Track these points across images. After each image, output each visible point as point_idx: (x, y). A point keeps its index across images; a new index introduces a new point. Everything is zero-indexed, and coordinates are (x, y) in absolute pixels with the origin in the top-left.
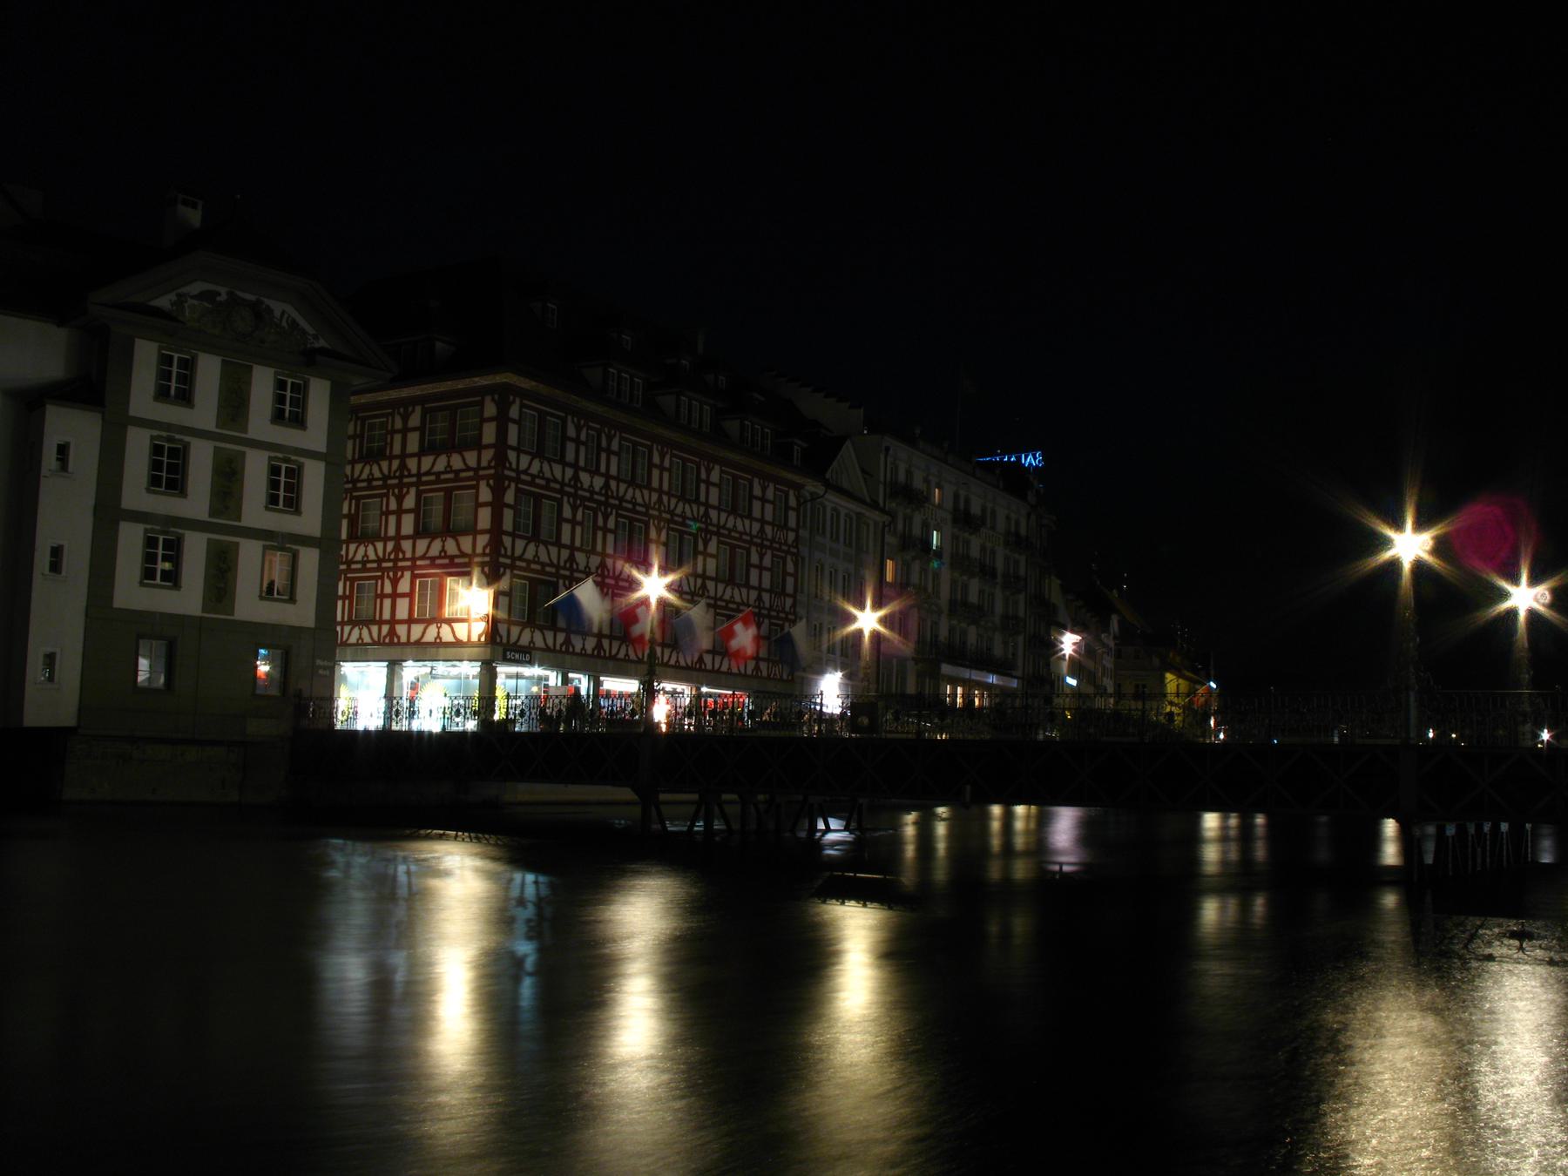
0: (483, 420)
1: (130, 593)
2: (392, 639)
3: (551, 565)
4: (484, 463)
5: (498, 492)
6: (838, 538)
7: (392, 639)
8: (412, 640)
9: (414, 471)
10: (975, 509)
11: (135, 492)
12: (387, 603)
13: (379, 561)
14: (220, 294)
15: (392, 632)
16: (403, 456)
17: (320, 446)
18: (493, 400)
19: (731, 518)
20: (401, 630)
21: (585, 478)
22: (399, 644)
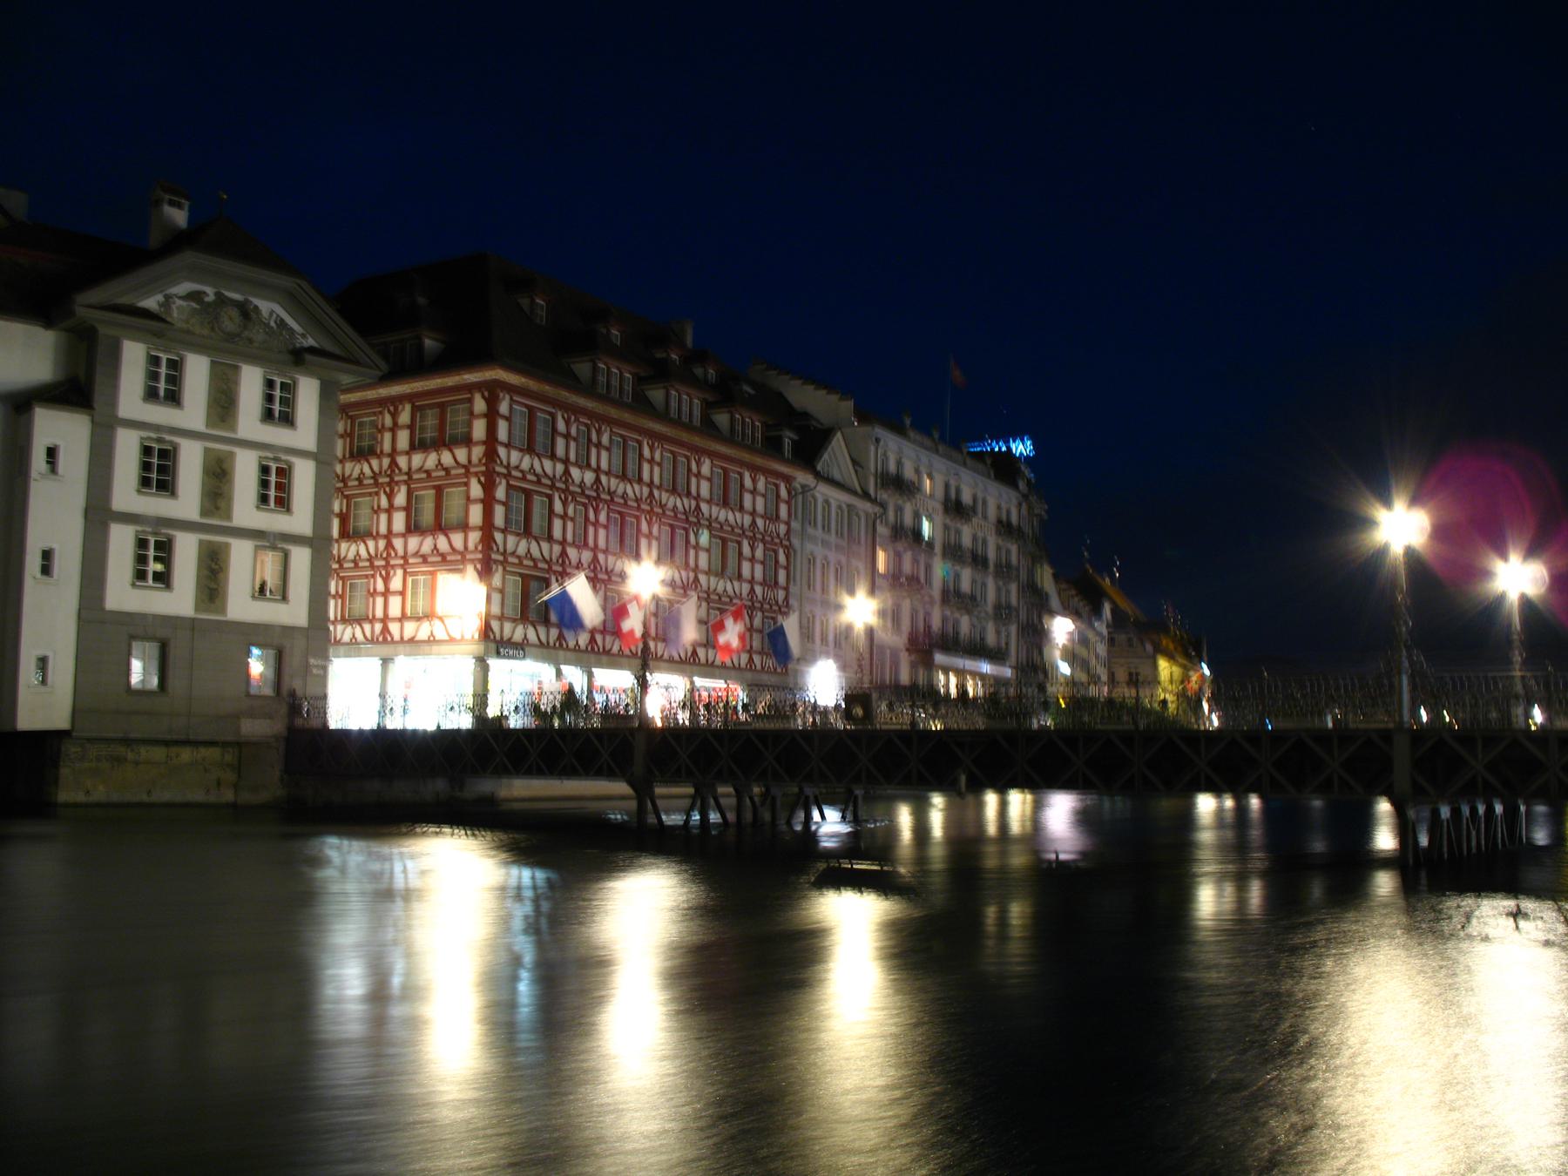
6: (829, 530)
8: (406, 638)
11: (126, 493)
12: (380, 601)
15: (385, 630)
18: (483, 397)
20: (394, 628)
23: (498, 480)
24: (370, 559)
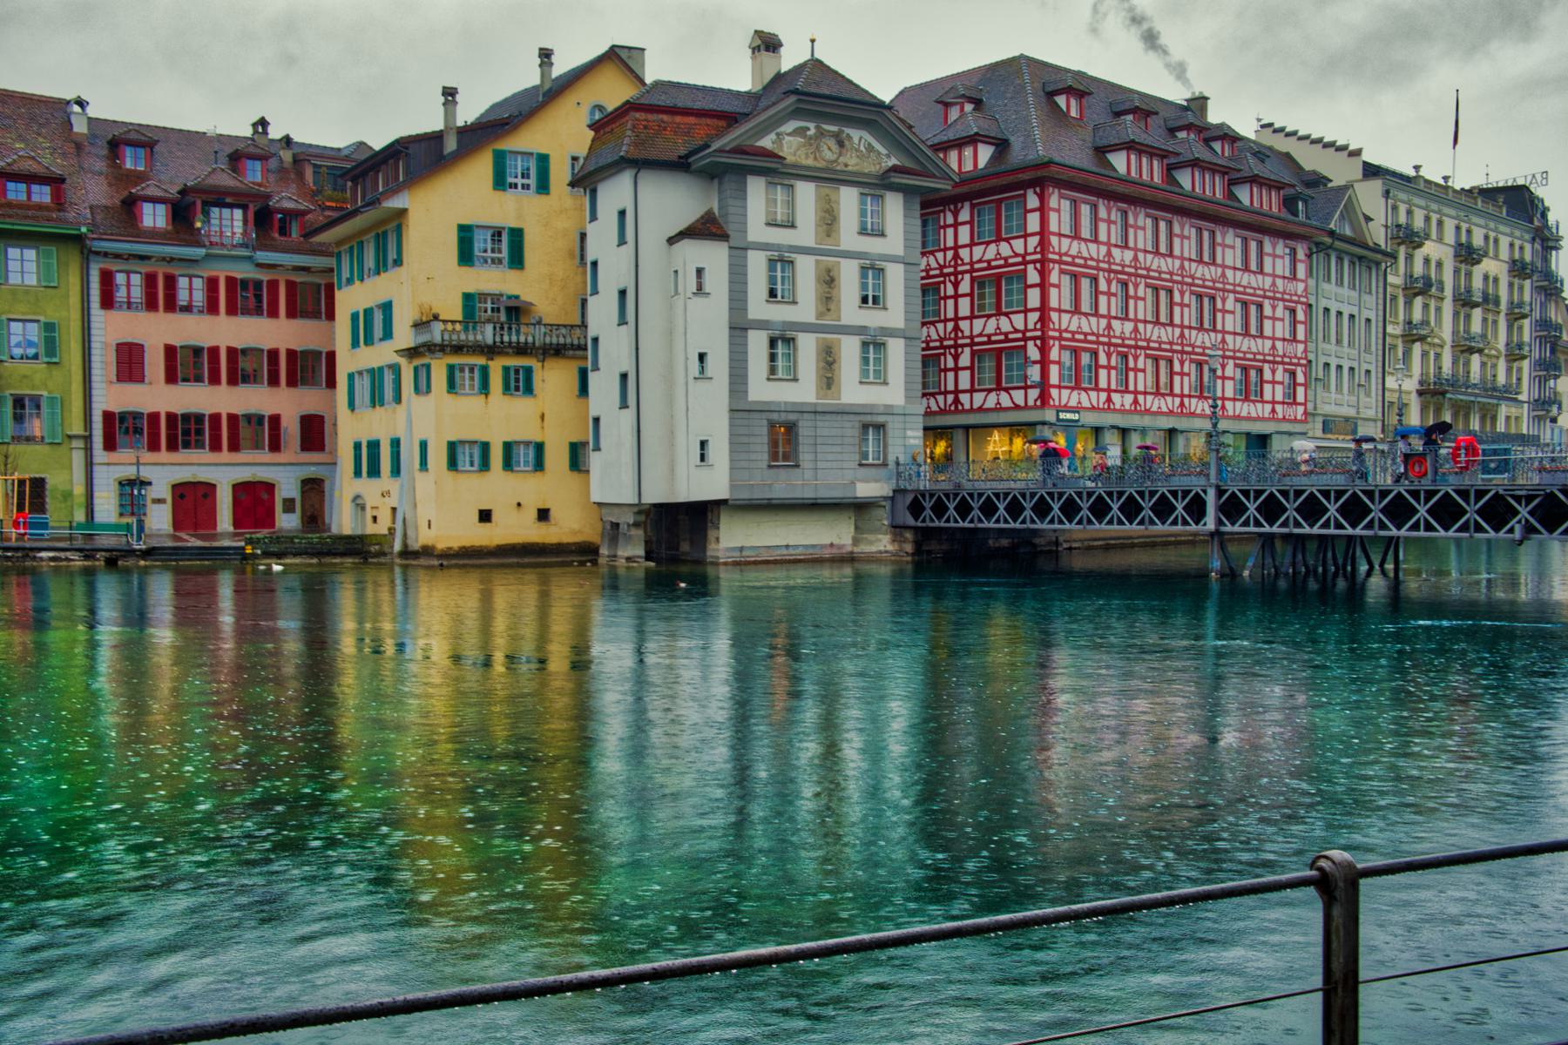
0: (1027, 211)
1: (761, 390)
2: (956, 407)
3: (1093, 334)
4: (1030, 250)
5: (1043, 274)
6: (1342, 283)
7: (956, 407)
8: (975, 407)
9: (967, 260)
10: (1478, 241)
11: (758, 306)
12: (951, 375)
13: (941, 340)
14: (809, 129)
15: (957, 401)
16: (956, 248)
17: (899, 250)
18: (1035, 193)
19: (1156, 260)
20: (964, 398)
21: (1116, 252)
22: (964, 411)
23: (1051, 342)
24: (941, 267)
